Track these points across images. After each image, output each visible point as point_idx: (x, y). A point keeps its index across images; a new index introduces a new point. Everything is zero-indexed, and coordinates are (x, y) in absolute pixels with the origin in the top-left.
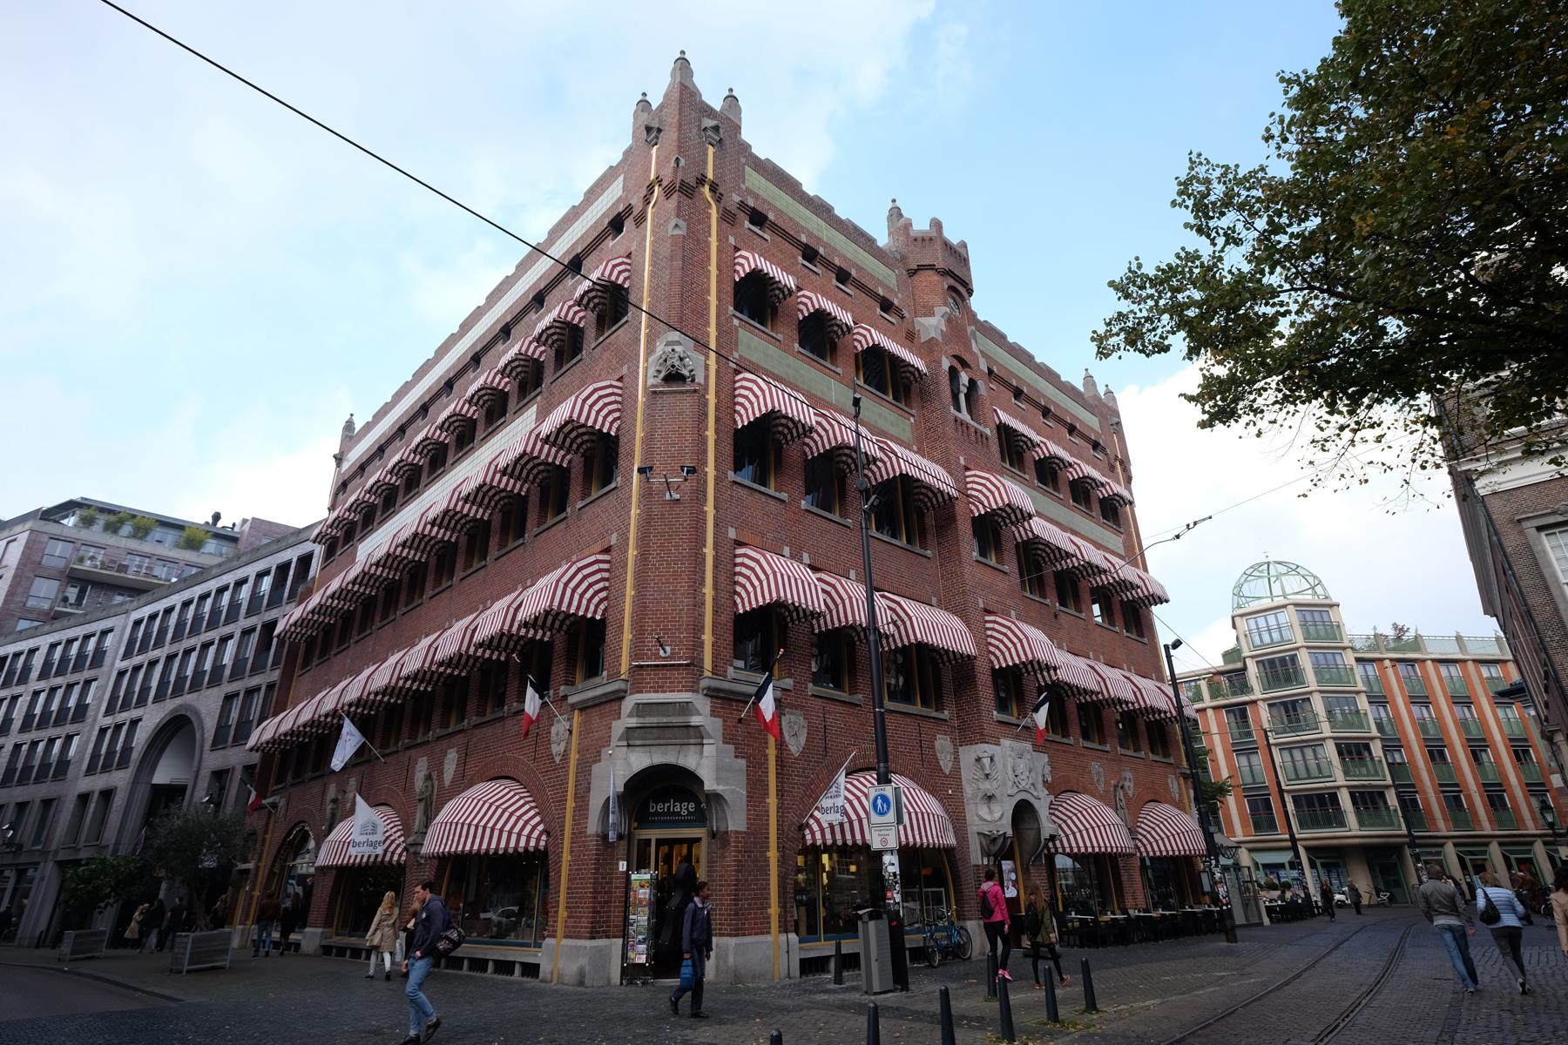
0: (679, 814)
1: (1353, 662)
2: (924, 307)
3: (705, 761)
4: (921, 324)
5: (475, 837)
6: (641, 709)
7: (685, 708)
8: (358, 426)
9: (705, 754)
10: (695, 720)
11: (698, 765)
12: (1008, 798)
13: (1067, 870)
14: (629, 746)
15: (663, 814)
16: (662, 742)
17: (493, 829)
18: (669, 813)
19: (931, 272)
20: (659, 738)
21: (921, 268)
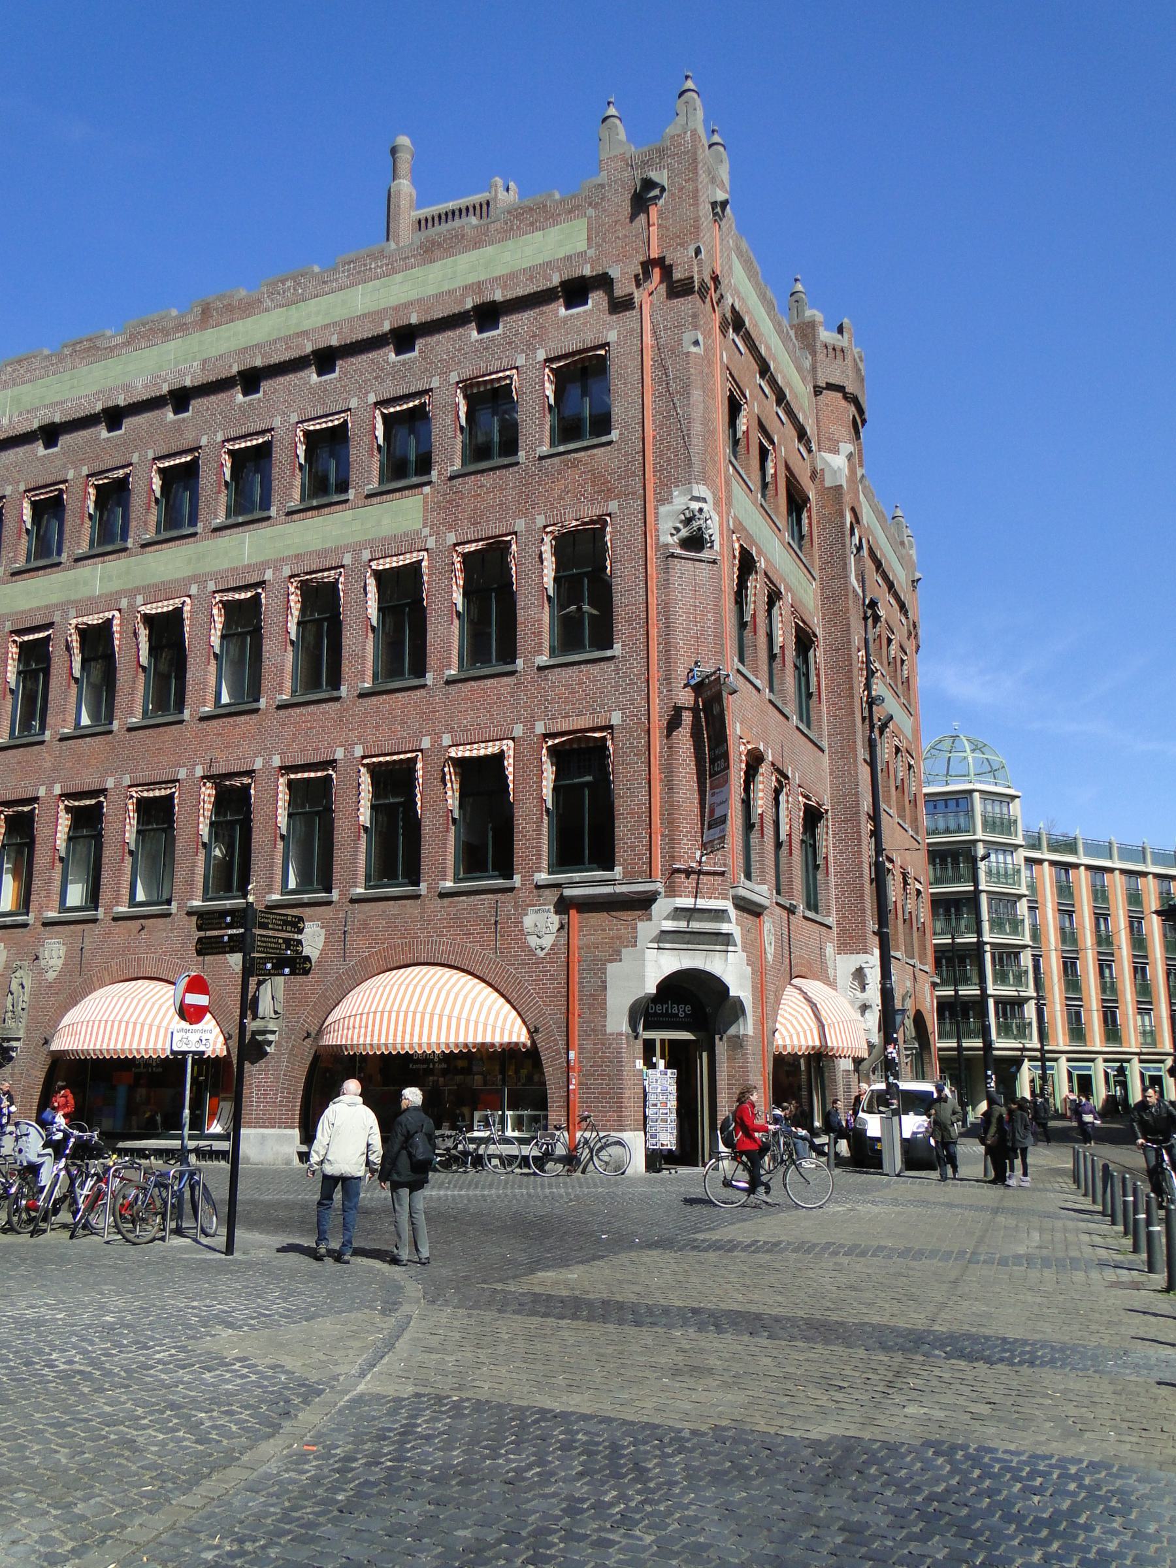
0: (676, 1015)
1: (1022, 862)
2: (830, 439)
3: (730, 968)
4: (826, 462)
5: (133, 1034)
6: (679, 913)
7: (719, 915)
8: (871, 813)
9: (730, 961)
10: (725, 928)
11: (724, 971)
12: (439, 902)
13: (621, 1035)
14: (659, 949)
15: (662, 1015)
16: (690, 946)
17: (151, 1026)
18: (667, 1014)
19: (840, 395)
20: (688, 943)
21: (830, 387)
